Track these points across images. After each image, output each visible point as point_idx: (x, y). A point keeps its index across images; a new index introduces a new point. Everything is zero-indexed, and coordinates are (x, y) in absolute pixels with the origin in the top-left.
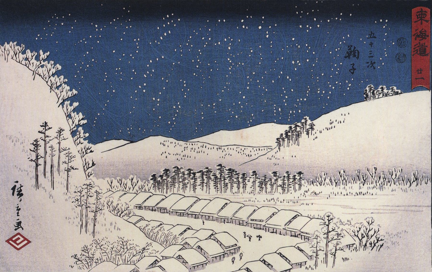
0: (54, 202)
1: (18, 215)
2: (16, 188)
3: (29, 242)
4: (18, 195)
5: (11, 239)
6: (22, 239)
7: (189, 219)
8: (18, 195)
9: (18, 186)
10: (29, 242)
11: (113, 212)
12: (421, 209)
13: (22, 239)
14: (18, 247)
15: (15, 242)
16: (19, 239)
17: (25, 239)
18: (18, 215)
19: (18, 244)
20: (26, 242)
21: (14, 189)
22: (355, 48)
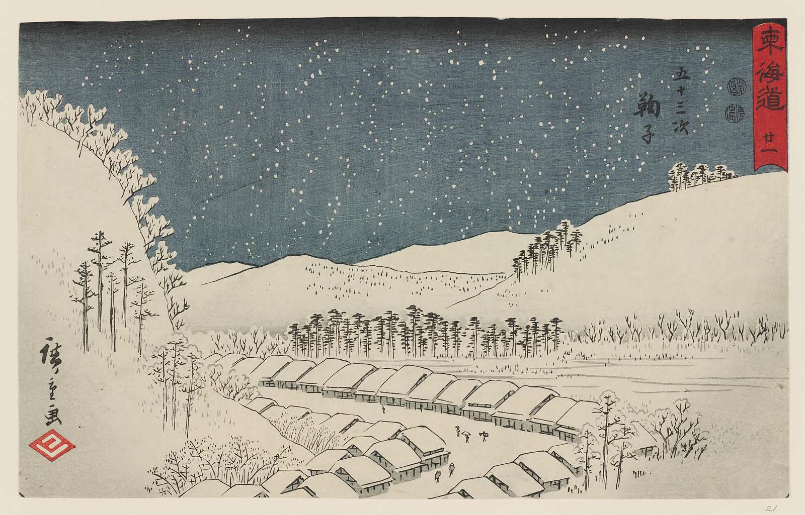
3: (71, 447)
6: (58, 441)
10: (71, 447)
13: (58, 441)
14: (52, 455)
15: (46, 446)
17: (64, 441)
19: (51, 451)
20: (65, 446)
21: (44, 351)
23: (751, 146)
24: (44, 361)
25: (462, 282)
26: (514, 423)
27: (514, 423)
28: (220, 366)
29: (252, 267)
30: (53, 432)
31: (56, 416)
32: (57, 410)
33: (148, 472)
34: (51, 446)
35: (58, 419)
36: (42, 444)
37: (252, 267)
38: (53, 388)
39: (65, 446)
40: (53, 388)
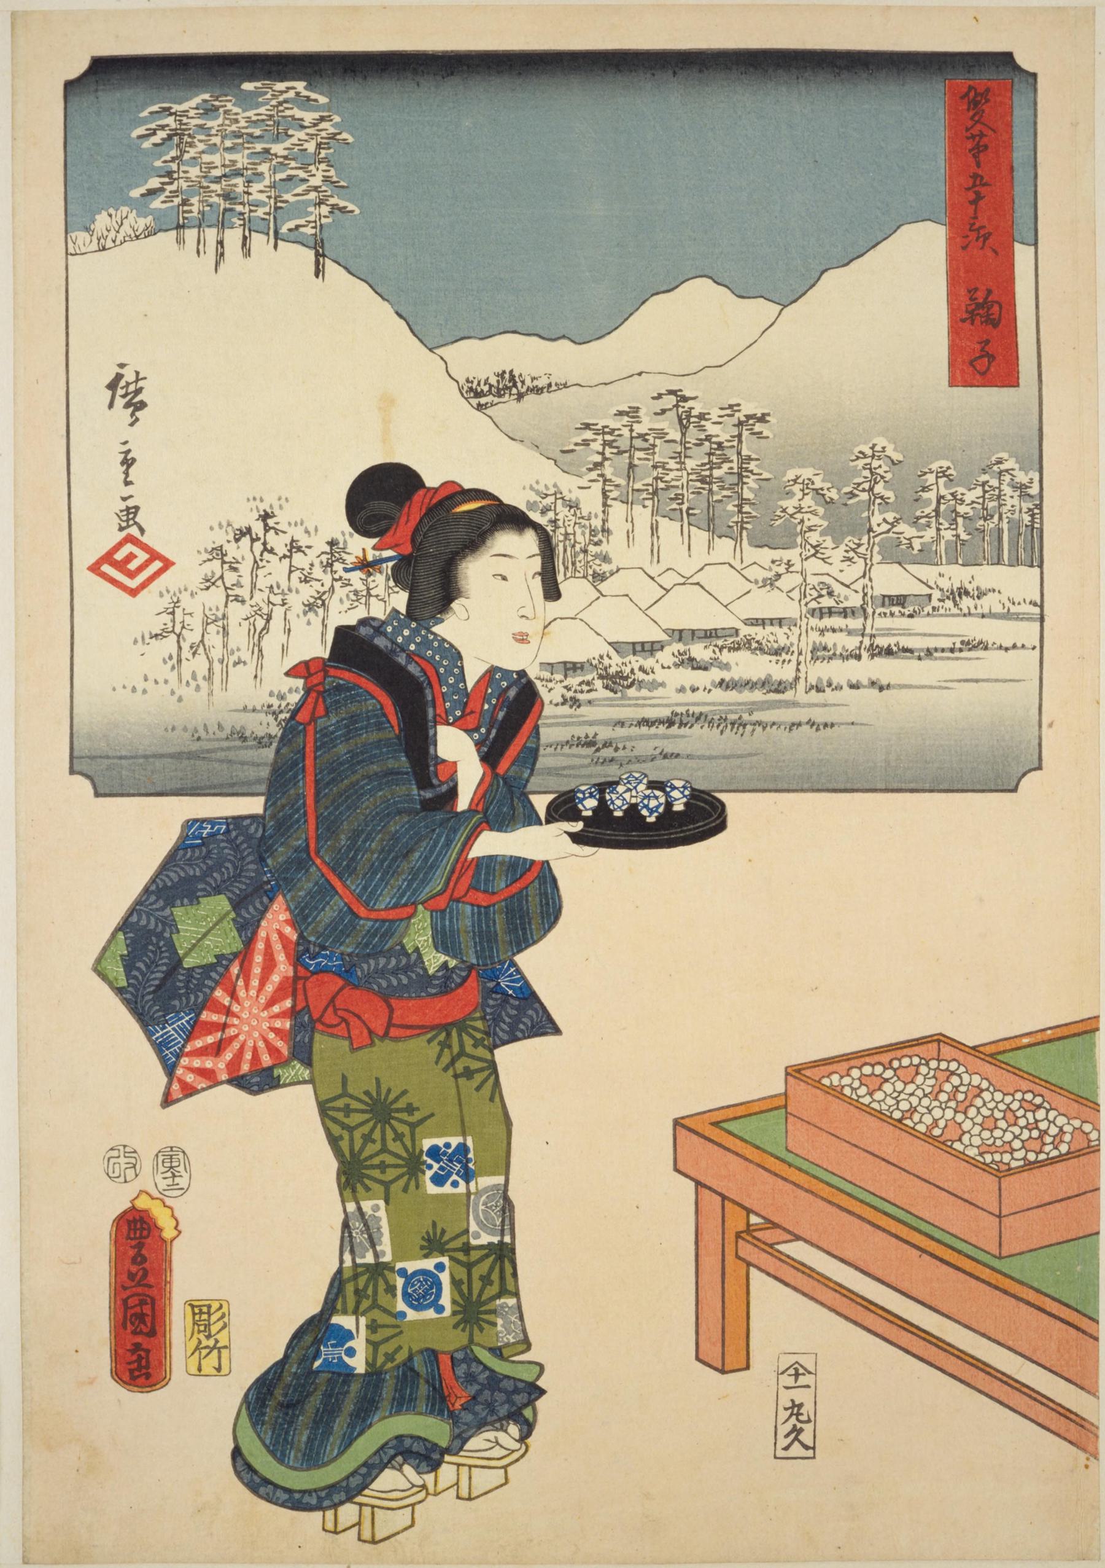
0: (504, 578)
1: (127, 483)
2: (122, 383)
3: (168, 564)
4: (127, 406)
5: (108, 557)
6: (142, 556)
7: (1101, 1026)
8: (127, 406)
9: (129, 376)
10: (168, 564)
11: (577, 575)
12: (939, 684)
13: (142, 556)
14: (133, 584)
15: (121, 566)
16: (131, 557)
17: (154, 556)
18: (127, 483)
19: (132, 575)
20: (157, 565)
21: (112, 386)
22: (989, 292)
23: (544, 714)
24: (111, 406)
25: (247, 233)
26: (808, 1386)
27: (808, 1386)
28: (538, 1368)
29: (497, 1095)
30: (130, 539)
31: (133, 519)
32: (137, 508)
33: (248, 500)
34: (133, 566)
35: (136, 523)
36: (115, 564)
37: (497, 1095)
38: (128, 462)
39: (157, 565)
40: (128, 462)
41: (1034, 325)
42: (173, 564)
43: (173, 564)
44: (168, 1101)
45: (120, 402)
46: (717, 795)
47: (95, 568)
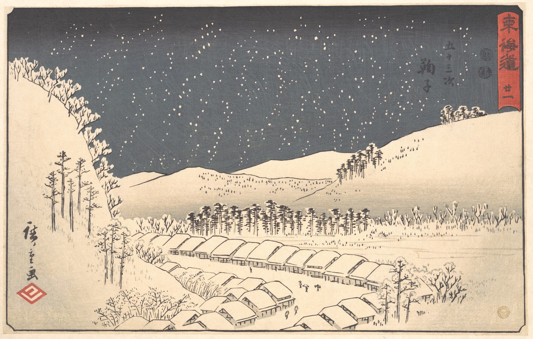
1: (31, 263)
2: (30, 230)
3: (44, 294)
5: (23, 291)
6: (36, 290)
9: (31, 227)
10: (44, 294)
13: (36, 290)
14: (32, 300)
15: (28, 294)
17: (40, 290)
18: (31, 263)
20: (41, 294)
21: (26, 231)
32: (34, 270)
38: (32, 255)
39: (41, 294)
40: (32, 255)
41: (521, 125)
42: (46, 294)
43: (46, 294)
44: (18, 293)
45: (29, 236)
46: (161, 175)
47: (19, 293)
